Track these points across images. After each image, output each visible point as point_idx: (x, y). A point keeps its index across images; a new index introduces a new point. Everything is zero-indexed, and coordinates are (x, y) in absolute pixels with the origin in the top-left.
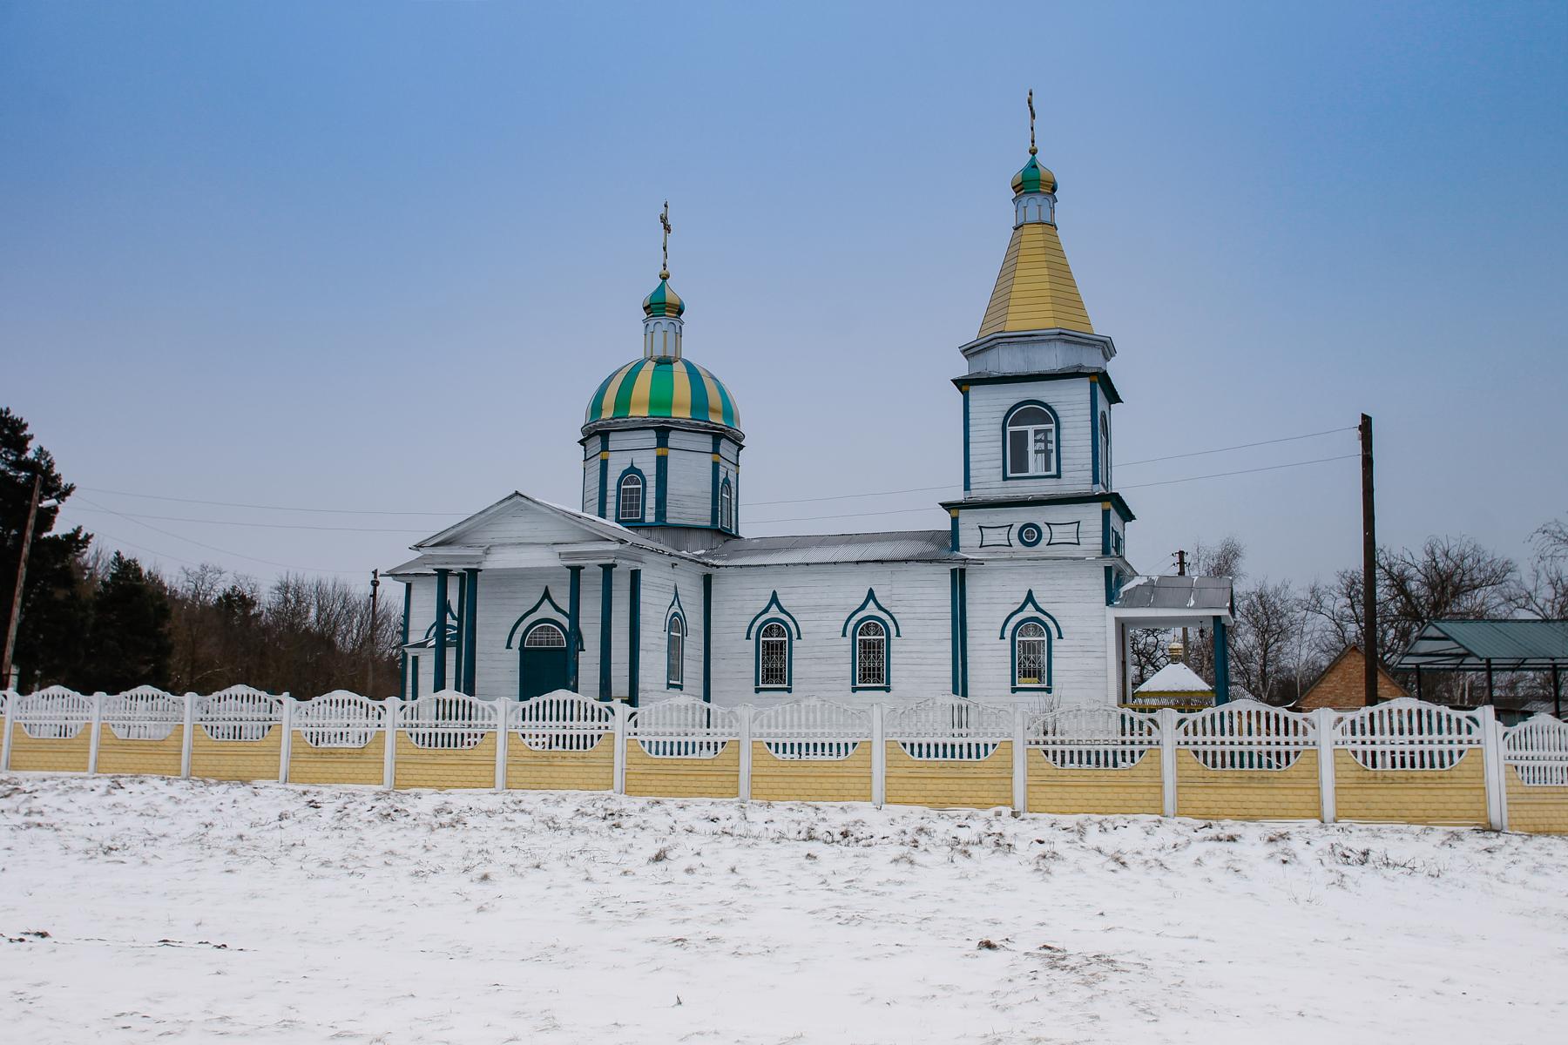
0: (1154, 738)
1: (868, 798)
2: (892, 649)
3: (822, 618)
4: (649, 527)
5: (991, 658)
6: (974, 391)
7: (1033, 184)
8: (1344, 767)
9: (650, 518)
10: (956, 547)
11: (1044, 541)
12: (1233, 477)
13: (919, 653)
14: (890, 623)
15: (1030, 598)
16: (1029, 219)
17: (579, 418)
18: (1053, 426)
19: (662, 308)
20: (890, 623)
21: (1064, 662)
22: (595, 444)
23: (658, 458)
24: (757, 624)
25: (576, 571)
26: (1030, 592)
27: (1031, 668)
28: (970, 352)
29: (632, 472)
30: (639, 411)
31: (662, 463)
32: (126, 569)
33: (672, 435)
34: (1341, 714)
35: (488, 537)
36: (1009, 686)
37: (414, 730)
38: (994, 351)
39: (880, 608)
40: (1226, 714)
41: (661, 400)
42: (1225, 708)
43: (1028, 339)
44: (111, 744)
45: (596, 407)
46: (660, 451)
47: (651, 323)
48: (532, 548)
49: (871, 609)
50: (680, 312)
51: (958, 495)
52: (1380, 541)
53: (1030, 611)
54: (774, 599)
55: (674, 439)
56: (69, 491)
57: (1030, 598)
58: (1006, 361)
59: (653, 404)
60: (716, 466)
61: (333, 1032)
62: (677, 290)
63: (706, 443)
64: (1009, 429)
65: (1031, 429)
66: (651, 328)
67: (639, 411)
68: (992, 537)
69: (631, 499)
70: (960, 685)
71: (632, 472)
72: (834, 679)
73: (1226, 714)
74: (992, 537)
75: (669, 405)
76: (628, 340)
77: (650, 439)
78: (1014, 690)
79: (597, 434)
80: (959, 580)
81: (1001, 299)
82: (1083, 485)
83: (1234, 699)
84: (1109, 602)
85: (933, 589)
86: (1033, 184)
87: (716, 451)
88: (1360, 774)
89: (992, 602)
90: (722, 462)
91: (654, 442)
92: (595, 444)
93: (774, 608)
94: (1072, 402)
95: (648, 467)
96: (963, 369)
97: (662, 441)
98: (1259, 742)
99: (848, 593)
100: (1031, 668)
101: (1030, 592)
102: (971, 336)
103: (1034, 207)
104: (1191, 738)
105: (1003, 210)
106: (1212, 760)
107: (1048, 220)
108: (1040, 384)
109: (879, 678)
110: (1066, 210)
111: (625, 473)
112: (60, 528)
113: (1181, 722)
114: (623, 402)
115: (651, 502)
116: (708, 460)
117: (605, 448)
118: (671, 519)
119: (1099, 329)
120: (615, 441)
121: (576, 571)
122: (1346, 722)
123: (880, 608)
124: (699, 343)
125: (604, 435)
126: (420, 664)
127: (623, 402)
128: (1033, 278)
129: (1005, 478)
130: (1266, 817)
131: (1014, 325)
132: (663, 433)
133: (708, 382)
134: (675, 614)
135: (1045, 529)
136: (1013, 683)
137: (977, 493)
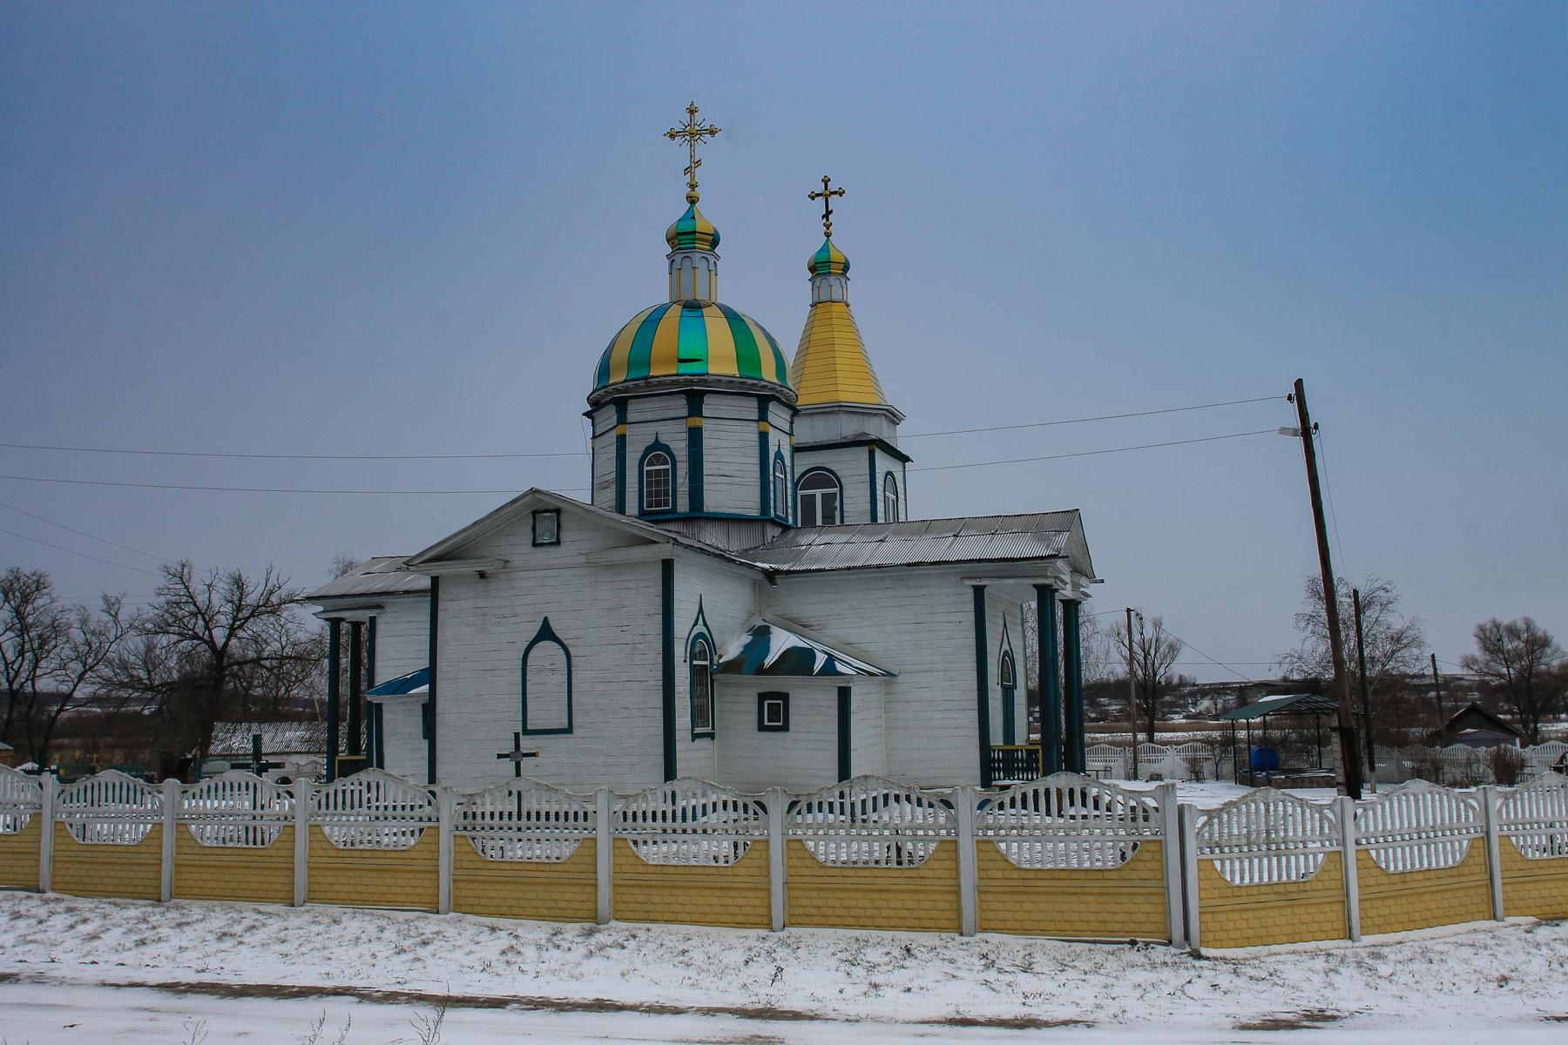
8: (798, 863)
9: (683, 506)
16: (823, 298)
17: (586, 384)
18: (836, 490)
19: (690, 241)
22: (609, 416)
29: (658, 449)
33: (707, 399)
40: (1042, 792)
45: (604, 370)
47: (678, 258)
48: (837, 438)
50: (715, 242)
52: (1337, 573)
55: (710, 406)
60: (763, 437)
62: (709, 216)
63: (749, 408)
66: (677, 264)
69: (658, 483)
70: (670, 773)
71: (658, 449)
73: (1042, 792)
77: (680, 406)
79: (611, 401)
87: (763, 417)
90: (771, 431)
91: (685, 413)
92: (609, 416)
94: (849, 467)
97: (695, 409)
111: (648, 450)
116: (751, 433)
117: (622, 420)
118: (865, 449)
120: (635, 411)
125: (621, 405)
130: (377, 902)
134: (701, 635)
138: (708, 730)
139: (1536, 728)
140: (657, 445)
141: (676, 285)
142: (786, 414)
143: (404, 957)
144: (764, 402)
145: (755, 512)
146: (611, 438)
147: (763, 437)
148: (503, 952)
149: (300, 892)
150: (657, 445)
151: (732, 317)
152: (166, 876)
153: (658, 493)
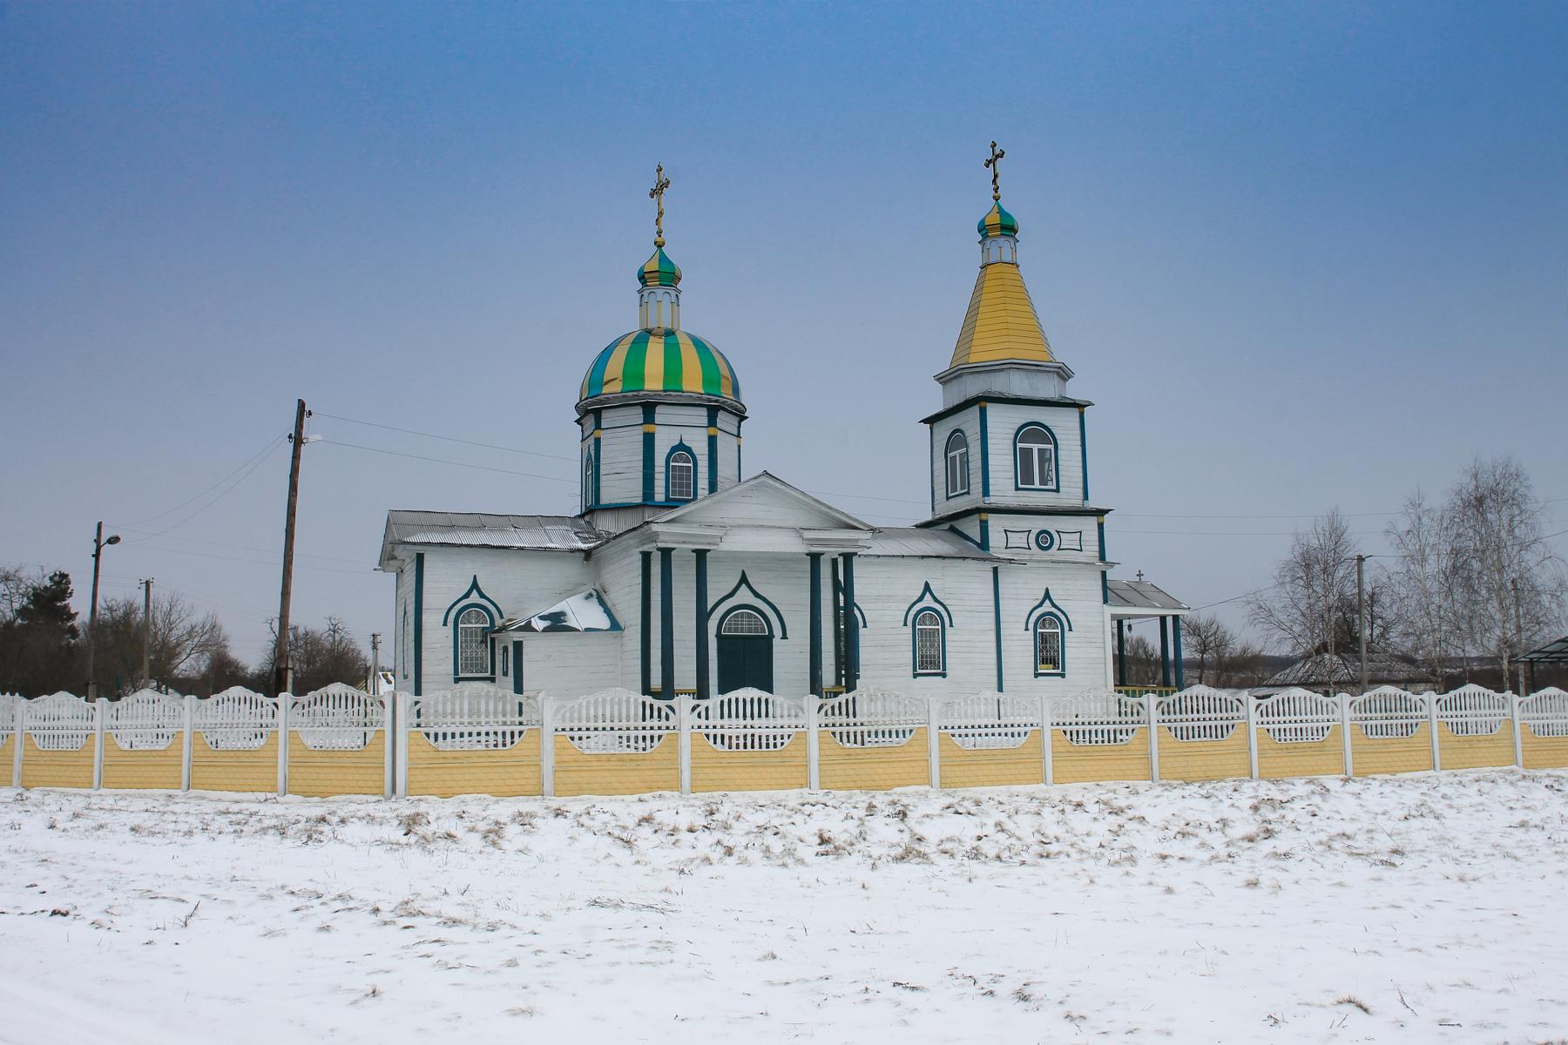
0: (671, 724)
1: (678, 787)
2: (947, 638)
5: (1020, 648)
11: (1056, 546)
12: (1206, 496)
13: (967, 644)
14: (945, 614)
15: (1047, 596)
19: (661, 276)
20: (945, 614)
21: (1075, 651)
23: (645, 434)
24: (913, 612)
26: (927, 585)
27: (1049, 656)
28: (944, 379)
29: (681, 448)
30: (693, 383)
31: (712, 441)
33: (659, 409)
34: (824, 701)
36: (1032, 671)
37: (1173, 725)
38: (1004, 374)
39: (936, 600)
42: (1182, 694)
44: (302, 760)
46: (712, 431)
47: (646, 293)
49: (928, 601)
53: (1047, 607)
57: (1047, 596)
58: (1018, 385)
59: (626, 376)
63: (637, 415)
64: (1019, 445)
65: (1035, 447)
66: (645, 299)
68: (1016, 540)
71: (681, 448)
72: (898, 666)
74: (1016, 540)
76: (622, 314)
77: (701, 416)
78: (1036, 675)
83: (1190, 685)
84: (1105, 601)
87: (712, 422)
88: (432, 755)
91: (705, 421)
92: (590, 421)
93: (475, 596)
94: (1062, 423)
97: (649, 418)
98: (1214, 719)
100: (1049, 656)
101: (927, 585)
103: (1001, 248)
104: (703, 722)
106: (1182, 734)
107: (1009, 259)
109: (934, 664)
110: (1028, 250)
111: (674, 449)
113: (821, 708)
117: (598, 426)
120: (661, 414)
121: (815, 558)
122: (828, 707)
123: (936, 600)
124: (695, 312)
125: (597, 414)
126: (525, 651)
129: (1017, 489)
131: (977, 357)
132: (649, 409)
135: (1056, 536)
136: (456, 672)
138: (488, 675)
139: (1423, 662)
140: (681, 446)
141: (644, 316)
142: (735, 420)
143: (1138, 814)
144: (713, 412)
145: (639, 500)
146: (591, 441)
147: (649, 440)
148: (1255, 808)
149: (548, 786)
150: (681, 446)
151: (698, 344)
152: (280, 777)
153: (681, 485)
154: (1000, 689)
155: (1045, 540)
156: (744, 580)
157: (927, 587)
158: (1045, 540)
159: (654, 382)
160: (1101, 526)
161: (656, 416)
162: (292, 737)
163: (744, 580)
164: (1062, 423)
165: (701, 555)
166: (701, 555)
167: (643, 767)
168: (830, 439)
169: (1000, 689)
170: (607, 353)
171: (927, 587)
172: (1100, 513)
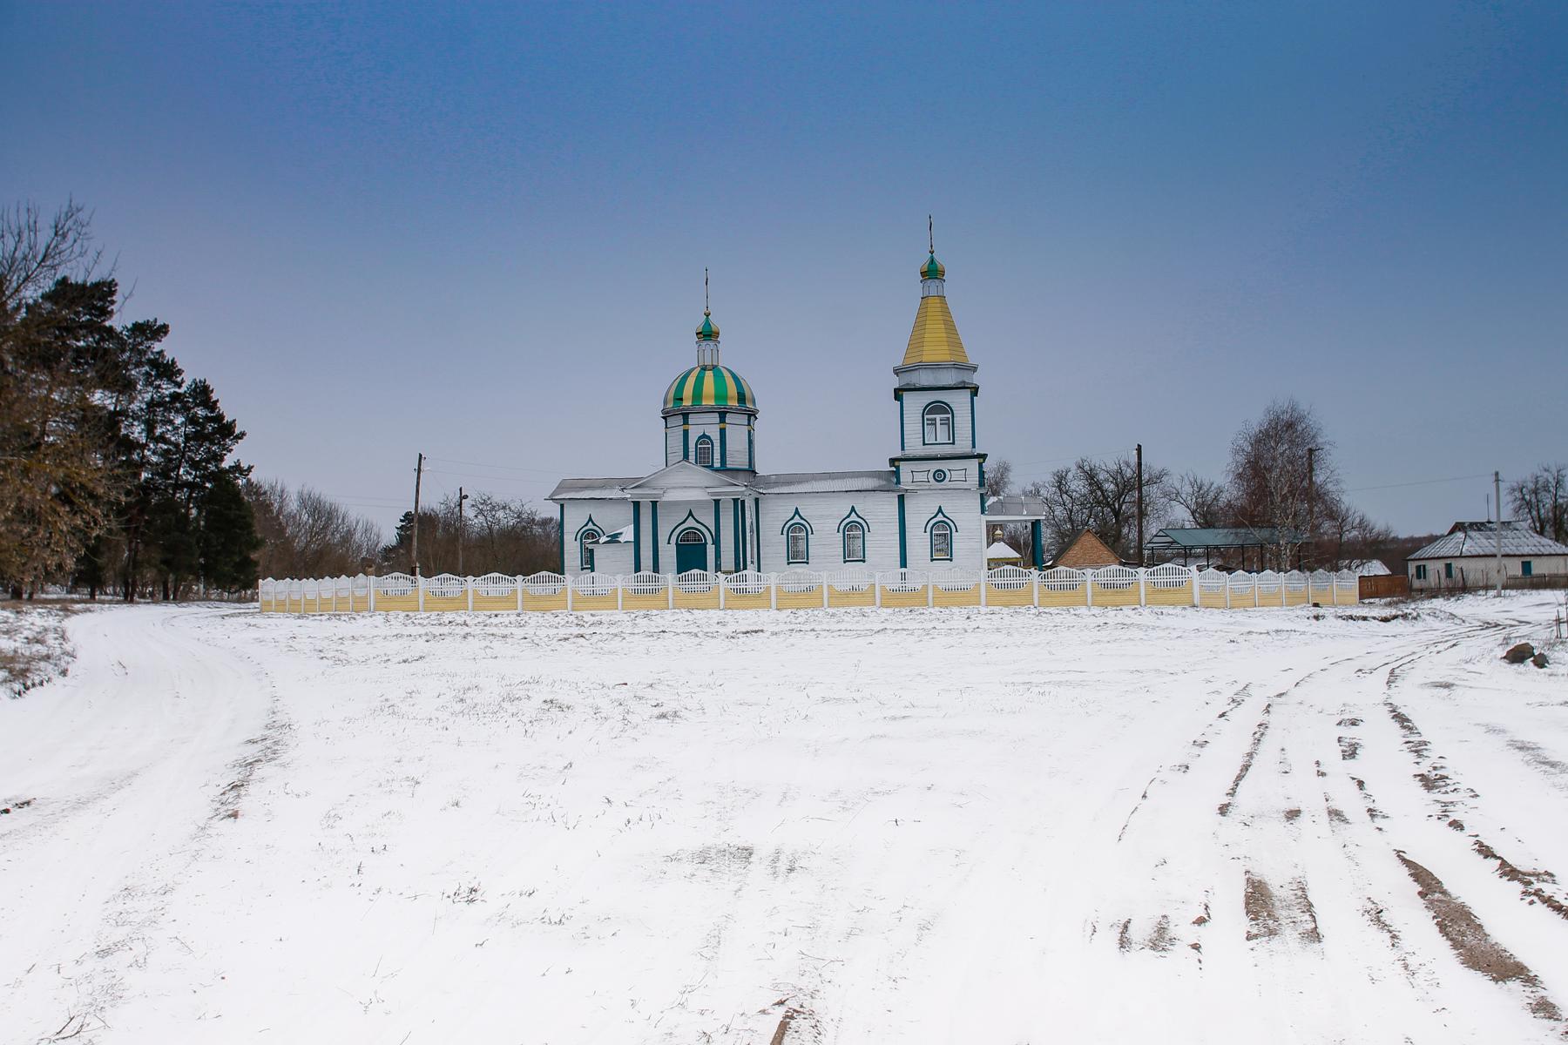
3: (825, 520)
4: (717, 470)
5: (919, 543)
6: (906, 395)
7: (932, 273)
9: (717, 464)
10: (898, 482)
13: (882, 540)
15: (940, 510)
19: (707, 334)
25: (717, 502)
28: (897, 372)
29: (704, 437)
30: (709, 402)
31: (723, 432)
32: (1337, 569)
35: (662, 483)
41: (721, 395)
43: (936, 367)
49: (853, 517)
51: (898, 454)
54: (797, 512)
56: (243, 434)
57: (940, 510)
58: (924, 378)
59: (717, 397)
61: (657, 711)
62: (717, 323)
65: (938, 417)
67: (709, 402)
68: (918, 477)
71: (704, 437)
74: (918, 477)
75: (726, 398)
76: (687, 355)
77: (715, 418)
80: (901, 499)
81: (916, 341)
82: (967, 449)
85: (889, 505)
86: (932, 273)
89: (920, 513)
94: (959, 401)
95: (715, 435)
96: (896, 382)
97: (722, 420)
99: (841, 508)
102: (899, 363)
103: (933, 285)
105: (916, 288)
108: (934, 386)
110: (951, 287)
112: (227, 463)
114: (698, 395)
115: (717, 456)
119: (972, 361)
120: (692, 419)
121: (717, 502)
124: (729, 355)
127: (698, 395)
128: (935, 330)
131: (928, 357)
132: (686, 416)
133: (726, 374)
137: (909, 452)
140: (704, 436)
147: (686, 433)
150: (704, 436)
154: (904, 564)
155: (939, 476)
156: (691, 514)
157: (853, 509)
158: (939, 476)
159: (687, 403)
160: (980, 465)
161: (707, 412)
162: (524, 592)
163: (691, 514)
164: (959, 401)
165: (654, 504)
166: (654, 504)
167: (647, 597)
168: (821, 416)
169: (904, 564)
170: (689, 372)
171: (853, 509)
172: (984, 456)
